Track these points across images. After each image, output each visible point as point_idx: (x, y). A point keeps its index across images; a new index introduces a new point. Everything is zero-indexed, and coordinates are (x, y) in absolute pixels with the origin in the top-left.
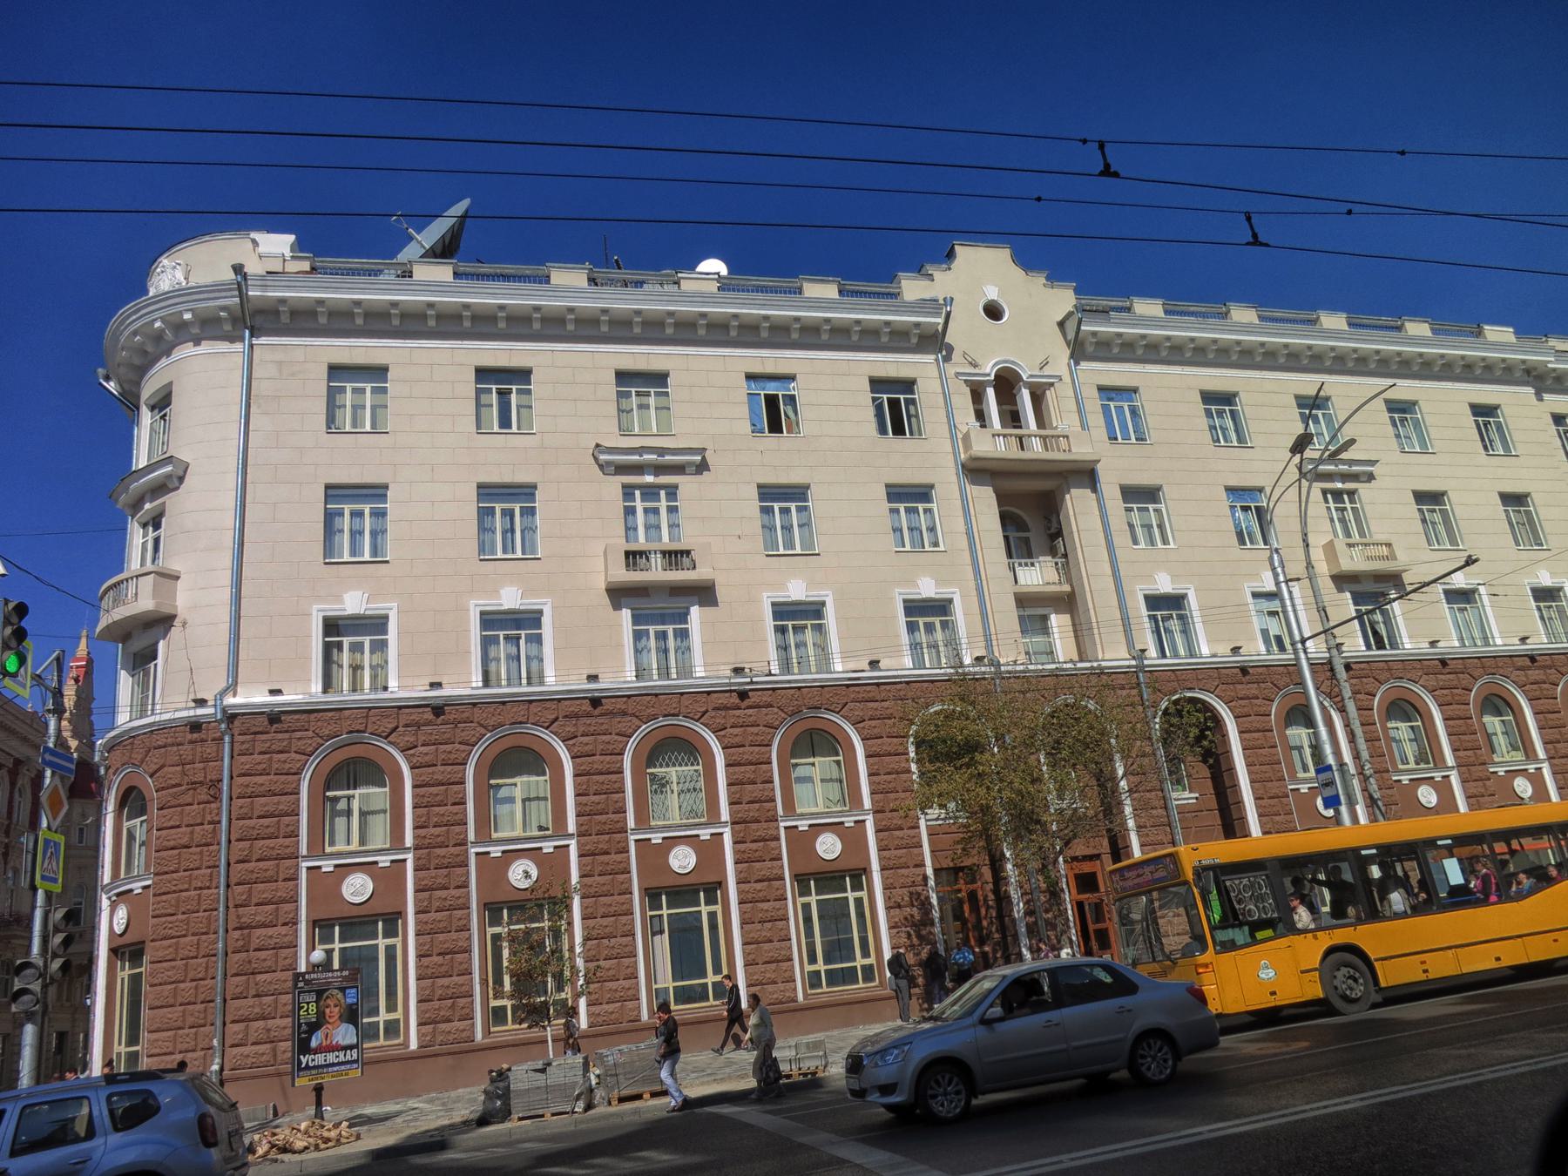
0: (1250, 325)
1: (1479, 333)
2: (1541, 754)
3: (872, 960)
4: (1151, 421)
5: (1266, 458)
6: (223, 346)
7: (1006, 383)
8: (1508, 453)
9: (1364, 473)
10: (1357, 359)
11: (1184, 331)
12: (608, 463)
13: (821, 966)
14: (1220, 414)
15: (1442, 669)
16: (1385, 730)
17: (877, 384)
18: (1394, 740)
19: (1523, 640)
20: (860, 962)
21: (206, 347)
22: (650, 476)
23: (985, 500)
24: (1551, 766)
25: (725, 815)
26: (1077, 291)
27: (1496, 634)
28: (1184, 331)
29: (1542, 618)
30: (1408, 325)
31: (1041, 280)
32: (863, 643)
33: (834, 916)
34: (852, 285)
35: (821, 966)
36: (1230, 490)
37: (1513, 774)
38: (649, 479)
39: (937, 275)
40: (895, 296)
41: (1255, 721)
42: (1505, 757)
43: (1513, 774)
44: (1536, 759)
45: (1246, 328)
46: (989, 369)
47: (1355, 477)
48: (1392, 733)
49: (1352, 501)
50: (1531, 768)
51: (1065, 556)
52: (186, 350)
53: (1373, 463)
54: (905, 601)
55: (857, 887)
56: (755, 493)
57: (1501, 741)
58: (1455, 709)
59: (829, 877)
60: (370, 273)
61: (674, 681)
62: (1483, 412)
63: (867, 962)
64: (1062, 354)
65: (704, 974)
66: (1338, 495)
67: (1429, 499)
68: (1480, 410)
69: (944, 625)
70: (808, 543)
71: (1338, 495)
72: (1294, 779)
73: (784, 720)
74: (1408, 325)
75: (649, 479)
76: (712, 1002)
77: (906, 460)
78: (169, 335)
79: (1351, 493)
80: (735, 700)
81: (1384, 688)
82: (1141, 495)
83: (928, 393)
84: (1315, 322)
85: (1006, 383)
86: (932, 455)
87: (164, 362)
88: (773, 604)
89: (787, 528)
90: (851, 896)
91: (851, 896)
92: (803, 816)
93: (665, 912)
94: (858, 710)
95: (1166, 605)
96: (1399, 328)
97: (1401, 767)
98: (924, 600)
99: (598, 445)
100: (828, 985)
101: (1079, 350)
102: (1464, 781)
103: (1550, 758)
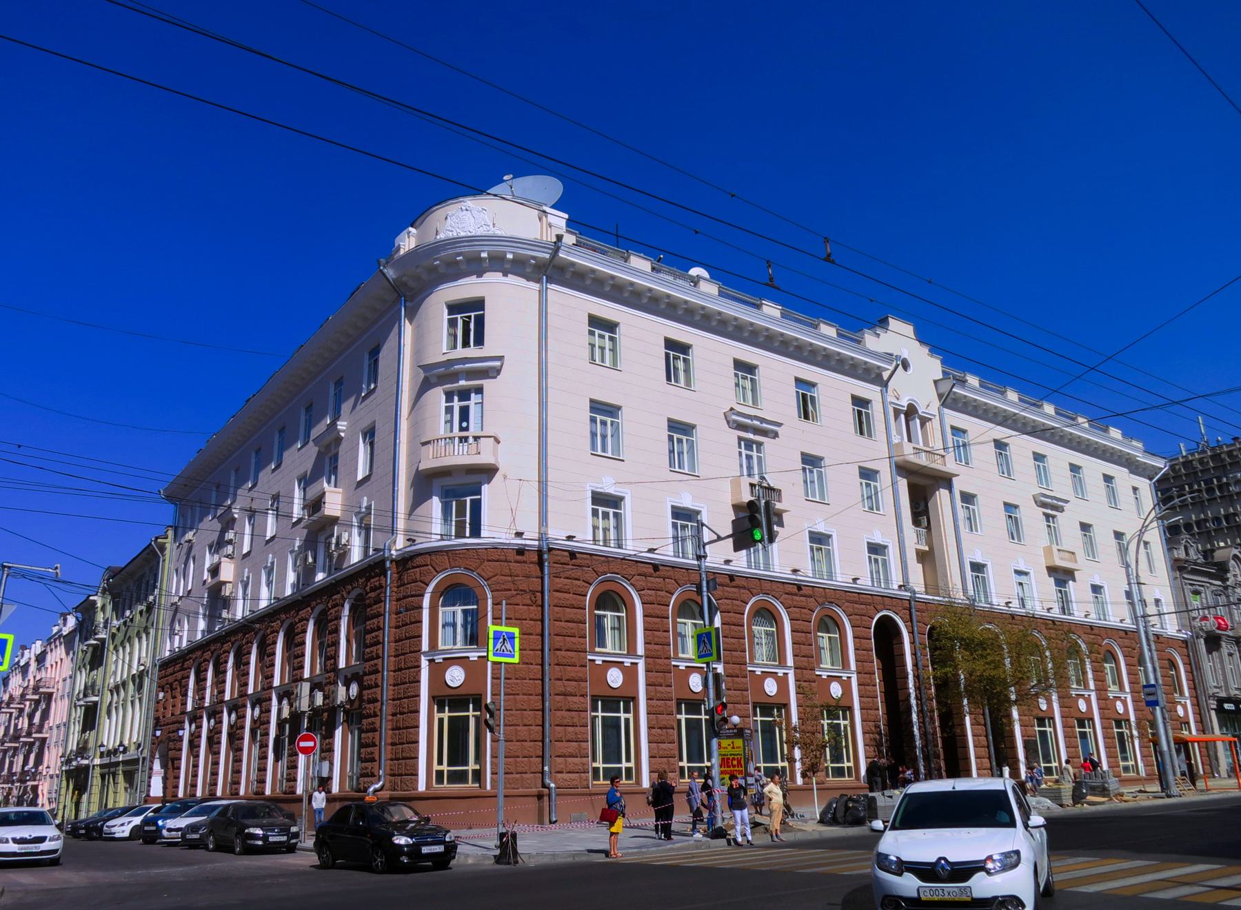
0: (830, 338)
1: (1106, 430)
2: (853, 666)
3: (632, 764)
4: (697, 374)
5: (1023, 488)
6: (521, 282)
7: (911, 412)
8: (614, 366)
9: (773, 431)
10: (736, 326)
11: (793, 331)
12: (735, 421)
13: (445, 767)
14: (601, 337)
15: (795, 591)
16: (675, 624)
17: (799, 381)
18: (680, 635)
19: (855, 580)
20: (624, 765)
21: (512, 279)
22: (753, 433)
23: (903, 484)
24: (647, 664)
25: (640, 650)
26: (943, 362)
27: (838, 571)
28: (793, 331)
29: (813, 559)
30: (822, 326)
31: (925, 350)
32: (849, 569)
33: (612, 727)
34: (585, 239)
35: (445, 767)
36: (1006, 504)
37: (766, 675)
38: (751, 436)
39: (882, 335)
40: (859, 342)
41: (657, 609)
42: (826, 667)
43: (766, 675)
44: (635, 655)
45: (1012, 403)
46: (904, 403)
47: (764, 433)
48: (680, 628)
49: (759, 451)
50: (781, 672)
51: (928, 528)
52: (493, 277)
53: (780, 425)
54: (673, 507)
55: (627, 711)
56: (587, 405)
57: (826, 655)
58: (657, 609)
59: (612, 701)
60: (603, 253)
61: (612, 549)
62: (676, 348)
63: (629, 765)
64: (936, 403)
65: (620, 762)
66: (749, 444)
67: (811, 461)
68: (671, 344)
69: (616, 515)
70: (617, 448)
71: (749, 444)
72: (752, 663)
73: (814, 605)
74: (822, 326)
75: (751, 436)
76: (602, 781)
77: (680, 403)
78: (486, 264)
79: (759, 444)
80: (795, 590)
81: (754, 600)
82: (968, 498)
83: (876, 410)
84: (816, 327)
85: (911, 412)
86: (876, 452)
87: (473, 279)
88: (673, 507)
89: (604, 437)
90: (623, 716)
91: (623, 716)
92: (758, 665)
93: (600, 714)
94: (641, 581)
95: (606, 502)
96: (758, 307)
97: (681, 655)
98: (684, 509)
99: (732, 409)
100: (449, 782)
101: (949, 401)
102: (647, 671)
103: (1097, 690)
